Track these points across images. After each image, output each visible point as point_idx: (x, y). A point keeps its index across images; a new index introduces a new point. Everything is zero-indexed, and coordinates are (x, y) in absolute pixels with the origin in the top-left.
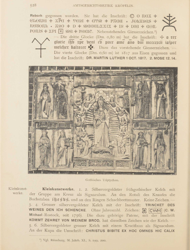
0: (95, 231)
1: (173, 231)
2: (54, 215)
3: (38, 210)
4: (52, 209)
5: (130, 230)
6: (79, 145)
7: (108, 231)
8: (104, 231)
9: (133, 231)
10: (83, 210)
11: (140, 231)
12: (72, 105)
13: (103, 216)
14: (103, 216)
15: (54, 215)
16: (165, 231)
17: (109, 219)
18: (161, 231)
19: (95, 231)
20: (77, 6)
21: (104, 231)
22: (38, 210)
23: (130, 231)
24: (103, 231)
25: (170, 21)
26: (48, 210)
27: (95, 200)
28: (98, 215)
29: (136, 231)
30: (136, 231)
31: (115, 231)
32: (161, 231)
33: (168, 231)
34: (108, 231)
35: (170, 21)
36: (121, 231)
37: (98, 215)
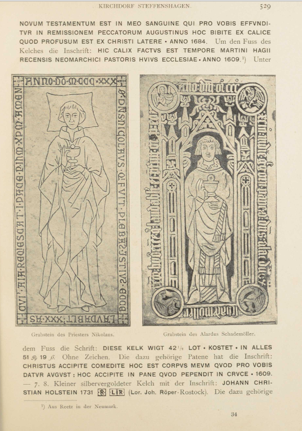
0: (232, 24)
1: (128, 50)
2: (196, 393)
3: (82, 34)
4: (78, 22)
5: (47, 391)
6: (251, 308)
7: (234, 23)
8: (50, 60)
9: (199, 32)
10: (130, 348)
11: (210, 23)
12: (170, 186)
13: (148, 358)
14: (148, 358)
15: (196, 393)
16: (116, 50)
17: (161, 362)
18: (107, 50)
19: (232, 24)
20: (128, 6)
21: (50, 60)
22: (82, 34)
23: (99, 50)
24: (184, 33)
25: (220, 211)
26: (25, 375)
27: (184, 392)
28: (138, 357)
29: (89, 375)
30: (204, 32)
31: (224, 32)
32: (107, 50)
33: (254, 33)
34: (234, 23)
35: (220, 211)
36: (160, 59)
37: (138, 357)
